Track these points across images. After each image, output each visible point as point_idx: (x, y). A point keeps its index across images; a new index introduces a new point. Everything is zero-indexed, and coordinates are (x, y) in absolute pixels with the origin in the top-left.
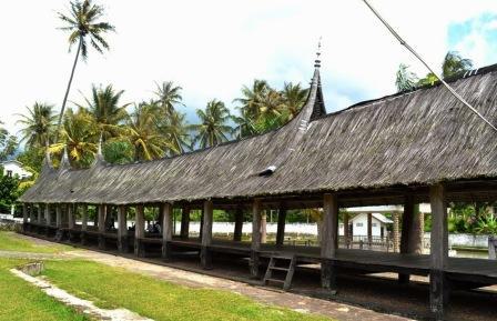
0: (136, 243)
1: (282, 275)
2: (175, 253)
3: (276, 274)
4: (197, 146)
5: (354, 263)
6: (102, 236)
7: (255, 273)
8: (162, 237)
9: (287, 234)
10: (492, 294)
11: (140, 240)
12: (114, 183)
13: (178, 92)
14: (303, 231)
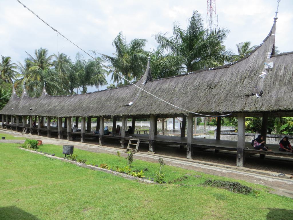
0: (68, 134)
1: (134, 147)
2: (86, 138)
3: (131, 146)
4: (236, 62)
5: (161, 141)
6: (49, 131)
7: (123, 146)
8: (121, 135)
9: (222, 131)
10: (291, 161)
11: (69, 133)
12: (59, 105)
13: (128, 42)
14: (143, 126)
